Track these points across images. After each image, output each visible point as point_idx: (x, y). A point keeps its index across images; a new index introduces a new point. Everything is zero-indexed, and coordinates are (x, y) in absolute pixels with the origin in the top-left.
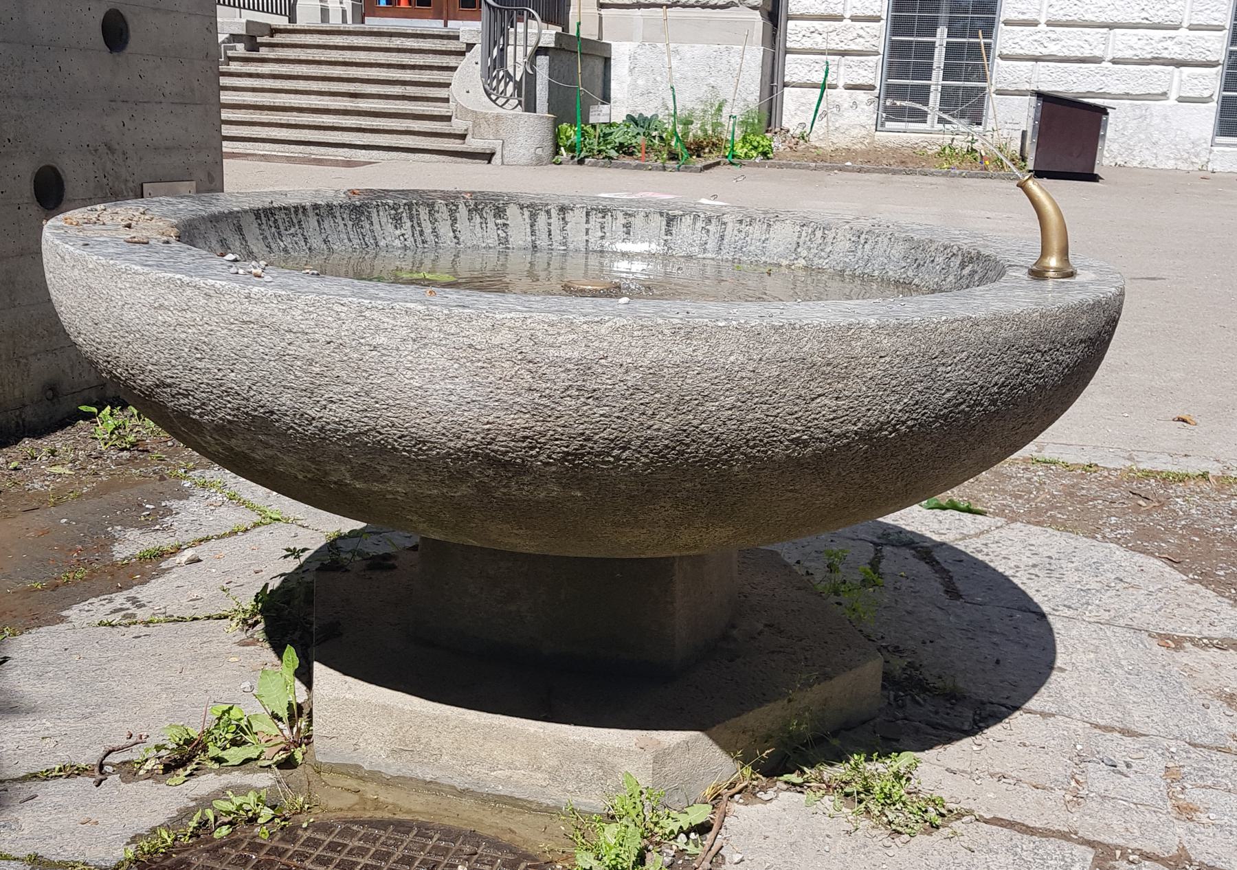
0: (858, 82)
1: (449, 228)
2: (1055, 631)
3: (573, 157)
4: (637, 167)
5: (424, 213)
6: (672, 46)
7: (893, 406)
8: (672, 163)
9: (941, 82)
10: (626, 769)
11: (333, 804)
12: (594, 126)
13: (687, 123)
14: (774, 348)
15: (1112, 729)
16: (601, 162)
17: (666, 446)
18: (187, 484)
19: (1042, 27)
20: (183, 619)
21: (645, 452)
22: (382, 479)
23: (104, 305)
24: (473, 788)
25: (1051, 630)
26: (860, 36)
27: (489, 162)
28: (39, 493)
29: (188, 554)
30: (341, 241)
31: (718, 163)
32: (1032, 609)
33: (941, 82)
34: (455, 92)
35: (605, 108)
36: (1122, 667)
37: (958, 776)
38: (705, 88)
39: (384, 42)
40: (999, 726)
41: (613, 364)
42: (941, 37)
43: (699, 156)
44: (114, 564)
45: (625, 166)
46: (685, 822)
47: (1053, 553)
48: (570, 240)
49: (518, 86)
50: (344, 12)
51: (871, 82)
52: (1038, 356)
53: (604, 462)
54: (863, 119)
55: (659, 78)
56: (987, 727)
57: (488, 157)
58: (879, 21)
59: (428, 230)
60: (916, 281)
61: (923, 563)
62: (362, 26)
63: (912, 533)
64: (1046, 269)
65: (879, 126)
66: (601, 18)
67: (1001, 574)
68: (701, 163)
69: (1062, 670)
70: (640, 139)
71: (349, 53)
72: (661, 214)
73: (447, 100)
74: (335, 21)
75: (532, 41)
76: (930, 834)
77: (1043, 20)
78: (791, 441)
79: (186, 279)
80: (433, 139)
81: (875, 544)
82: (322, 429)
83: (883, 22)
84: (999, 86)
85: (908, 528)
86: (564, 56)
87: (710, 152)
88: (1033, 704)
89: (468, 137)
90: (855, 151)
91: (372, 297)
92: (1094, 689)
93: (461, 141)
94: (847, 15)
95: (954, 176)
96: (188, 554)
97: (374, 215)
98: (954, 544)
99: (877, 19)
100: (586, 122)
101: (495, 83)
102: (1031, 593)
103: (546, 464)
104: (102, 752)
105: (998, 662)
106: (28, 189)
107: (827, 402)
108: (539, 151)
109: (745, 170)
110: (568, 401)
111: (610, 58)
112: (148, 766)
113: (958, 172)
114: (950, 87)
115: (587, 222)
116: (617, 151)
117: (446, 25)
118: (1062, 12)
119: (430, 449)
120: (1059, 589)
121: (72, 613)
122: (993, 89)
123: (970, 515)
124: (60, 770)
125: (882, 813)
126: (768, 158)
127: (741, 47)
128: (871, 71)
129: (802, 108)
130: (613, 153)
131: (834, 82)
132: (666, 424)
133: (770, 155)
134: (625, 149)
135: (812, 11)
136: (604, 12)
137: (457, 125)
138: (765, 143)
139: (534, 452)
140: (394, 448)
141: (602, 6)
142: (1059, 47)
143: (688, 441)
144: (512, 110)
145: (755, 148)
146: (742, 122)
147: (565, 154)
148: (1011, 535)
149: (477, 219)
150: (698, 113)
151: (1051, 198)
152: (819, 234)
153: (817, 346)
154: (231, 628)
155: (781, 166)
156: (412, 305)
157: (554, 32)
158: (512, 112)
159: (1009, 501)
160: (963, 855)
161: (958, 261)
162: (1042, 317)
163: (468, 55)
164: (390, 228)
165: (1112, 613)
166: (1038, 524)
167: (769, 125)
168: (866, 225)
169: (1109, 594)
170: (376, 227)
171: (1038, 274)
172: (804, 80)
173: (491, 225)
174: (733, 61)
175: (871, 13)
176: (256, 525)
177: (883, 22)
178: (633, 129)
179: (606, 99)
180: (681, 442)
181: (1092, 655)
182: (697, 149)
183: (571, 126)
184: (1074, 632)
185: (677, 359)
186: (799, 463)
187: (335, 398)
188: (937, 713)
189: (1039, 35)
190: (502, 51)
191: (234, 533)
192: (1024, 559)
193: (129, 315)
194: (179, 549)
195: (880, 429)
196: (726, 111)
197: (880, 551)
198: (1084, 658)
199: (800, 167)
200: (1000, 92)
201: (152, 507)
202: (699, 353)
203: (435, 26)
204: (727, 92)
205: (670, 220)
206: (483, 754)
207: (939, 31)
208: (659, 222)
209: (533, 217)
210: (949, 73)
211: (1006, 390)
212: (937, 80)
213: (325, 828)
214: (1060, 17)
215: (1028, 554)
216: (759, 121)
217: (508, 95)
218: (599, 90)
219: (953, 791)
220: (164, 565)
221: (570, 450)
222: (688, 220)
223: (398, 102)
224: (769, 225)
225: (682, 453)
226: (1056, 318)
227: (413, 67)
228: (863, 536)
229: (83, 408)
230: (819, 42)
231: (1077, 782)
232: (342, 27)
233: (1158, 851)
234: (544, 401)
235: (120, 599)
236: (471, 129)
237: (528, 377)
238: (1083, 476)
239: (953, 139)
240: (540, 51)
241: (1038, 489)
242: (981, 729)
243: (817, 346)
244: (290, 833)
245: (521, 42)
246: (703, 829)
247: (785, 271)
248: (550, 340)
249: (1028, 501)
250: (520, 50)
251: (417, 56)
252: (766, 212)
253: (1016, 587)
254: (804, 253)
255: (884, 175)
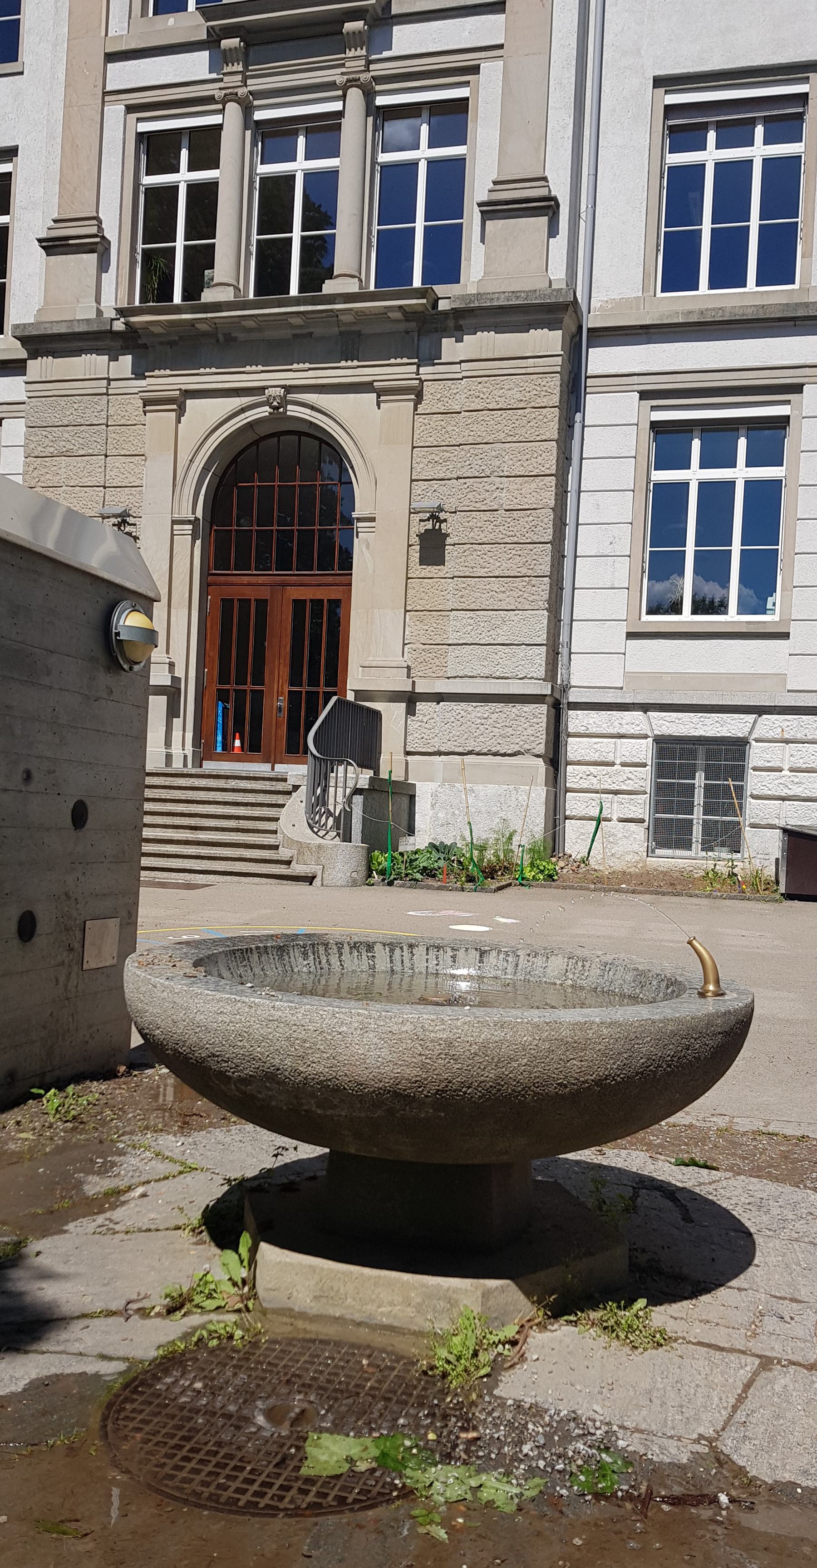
0: (630, 816)
1: (337, 959)
2: (757, 1243)
3: (383, 880)
4: (439, 888)
5: (321, 949)
6: (468, 786)
7: (609, 1067)
8: (470, 885)
9: (702, 817)
10: (465, 1302)
11: (277, 1330)
12: (402, 854)
13: (482, 849)
14: (547, 1033)
15: (785, 1298)
16: (408, 883)
17: (491, 1086)
18: (121, 1146)
19: (786, 772)
20: (149, 1230)
21: (480, 1089)
22: (334, 1107)
23: (184, 1012)
24: (367, 1320)
25: (754, 1243)
26: (629, 779)
27: (311, 884)
28: (13, 1153)
29: (140, 1190)
30: (272, 969)
31: (510, 885)
32: (744, 1230)
33: (702, 817)
34: (283, 825)
35: (411, 839)
36: (800, 1265)
37: (678, 1321)
38: (498, 820)
39: (221, 784)
40: (709, 1295)
41: (464, 1041)
42: (700, 780)
43: (493, 878)
44: (88, 1198)
45: (429, 887)
46: (502, 1336)
47: (765, 1196)
48: (416, 966)
49: (337, 820)
50: (185, 757)
51: (641, 816)
52: (692, 1040)
53: (457, 1095)
54: (636, 847)
55: (457, 812)
56: (701, 1295)
57: (310, 879)
58: (645, 767)
59: (324, 961)
60: (641, 996)
61: (668, 1201)
62: (199, 770)
63: (662, 1181)
64: (708, 991)
65: (650, 852)
66: (407, 763)
67: (725, 1209)
68: (495, 885)
69: (757, 1266)
70: (441, 863)
71: (190, 792)
72: (476, 949)
73: (275, 832)
74: (177, 765)
75: (351, 784)
76: (657, 1349)
77: (786, 767)
78: (558, 1084)
79: (238, 998)
80: (263, 865)
81: (633, 1188)
82: (306, 1079)
83: (648, 768)
84: (752, 821)
85: (659, 1178)
86: (376, 796)
87: (502, 874)
88: (734, 1283)
89: (293, 863)
90: (630, 873)
91: (339, 1007)
92: (777, 1277)
93: (286, 866)
94: (618, 762)
95: (716, 897)
96: (140, 1190)
97: (291, 952)
98: (691, 1189)
99: (644, 765)
100: (395, 849)
101: (317, 818)
102: (744, 1221)
103: (426, 1096)
104: (124, 1302)
105: (713, 1260)
106: (13, 927)
107: (575, 1062)
108: (354, 875)
109: (533, 890)
110: (440, 1061)
111: (414, 796)
112: (157, 1309)
113: (719, 894)
114: (710, 820)
115: (427, 954)
116: (422, 874)
117: (273, 769)
118: (801, 761)
119: (364, 1088)
120: (765, 1218)
121: (71, 1226)
122: (747, 823)
123: (706, 1170)
124: (100, 1313)
125: (627, 1337)
126: (554, 880)
127: (528, 788)
128: (641, 807)
129: (582, 837)
130: (418, 876)
131: (609, 816)
132: (491, 1074)
133: (556, 878)
134: (429, 873)
135: (587, 759)
136: (409, 758)
137: (284, 853)
138: (551, 867)
139: (420, 1090)
140: (345, 1088)
141: (408, 753)
142: (801, 789)
143: (503, 1083)
144: (331, 841)
145: (542, 872)
146: (530, 849)
147: (376, 876)
148: (735, 1183)
149: (356, 953)
150: (491, 841)
151: (705, 949)
152: (580, 964)
153: (569, 1032)
154: (186, 1234)
155: (564, 888)
156: (361, 1011)
157: (368, 776)
158: (331, 842)
159: (738, 1161)
160: (677, 1360)
161: (664, 984)
162: (692, 1019)
163: (294, 794)
164: (301, 960)
165: (801, 1234)
166: (758, 1177)
167: (554, 851)
168: (609, 958)
169: (801, 1222)
170: (292, 959)
171: (702, 995)
172: (583, 813)
173: (364, 957)
174: (520, 799)
175: (638, 760)
176: (181, 1173)
177: (648, 768)
178: (435, 855)
179: (411, 831)
180: (499, 1084)
181: (780, 1258)
182: (491, 872)
183: (382, 853)
184: (771, 1245)
185: (497, 1039)
186: (563, 1097)
187: (316, 1060)
188: (668, 1286)
189: (784, 779)
190: (325, 790)
191: (166, 1178)
192: (743, 1199)
193: (199, 1017)
194: (129, 1189)
195: (606, 1079)
196: (516, 840)
197: (638, 1193)
198: (772, 1260)
199: (581, 888)
200: (753, 826)
201: (101, 1161)
202: (508, 1036)
203: (262, 768)
204: (516, 824)
205: (482, 953)
206: (373, 1297)
207: (697, 774)
208: (474, 955)
209: (392, 951)
210: (708, 809)
211: (675, 1059)
212: (698, 815)
213: (275, 1342)
214: (800, 764)
215: (746, 1196)
216: (544, 848)
217: (328, 828)
218: (405, 823)
219: (672, 1327)
220: (122, 1199)
221: (440, 1088)
222: (494, 953)
223: (232, 834)
224: (548, 958)
225: (499, 1090)
226: (701, 1020)
227: (246, 804)
228: (625, 1182)
229: (34, 1091)
230: (594, 784)
231: (756, 1326)
232: (185, 771)
233: (801, 1360)
234: (428, 1061)
235: (100, 1219)
236: (295, 856)
237: (420, 1048)
238: (797, 1145)
239: (715, 865)
240: (357, 791)
241: (761, 1154)
242: (696, 1297)
243: (569, 1032)
244: (255, 1345)
245: (340, 784)
246: (514, 1343)
247: (558, 987)
248: (431, 1028)
249: (752, 1162)
250: (340, 791)
251: (250, 795)
252: (545, 949)
253: (733, 1217)
254: (571, 976)
255: (654, 896)
